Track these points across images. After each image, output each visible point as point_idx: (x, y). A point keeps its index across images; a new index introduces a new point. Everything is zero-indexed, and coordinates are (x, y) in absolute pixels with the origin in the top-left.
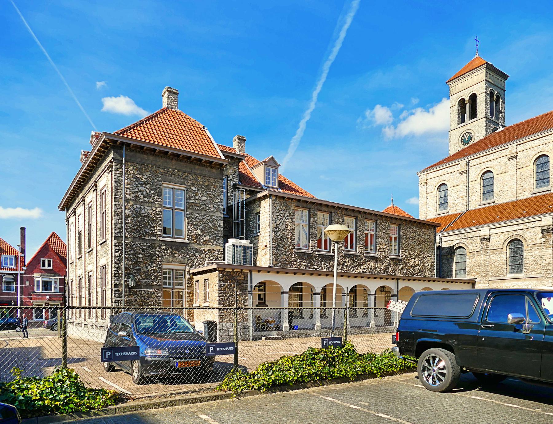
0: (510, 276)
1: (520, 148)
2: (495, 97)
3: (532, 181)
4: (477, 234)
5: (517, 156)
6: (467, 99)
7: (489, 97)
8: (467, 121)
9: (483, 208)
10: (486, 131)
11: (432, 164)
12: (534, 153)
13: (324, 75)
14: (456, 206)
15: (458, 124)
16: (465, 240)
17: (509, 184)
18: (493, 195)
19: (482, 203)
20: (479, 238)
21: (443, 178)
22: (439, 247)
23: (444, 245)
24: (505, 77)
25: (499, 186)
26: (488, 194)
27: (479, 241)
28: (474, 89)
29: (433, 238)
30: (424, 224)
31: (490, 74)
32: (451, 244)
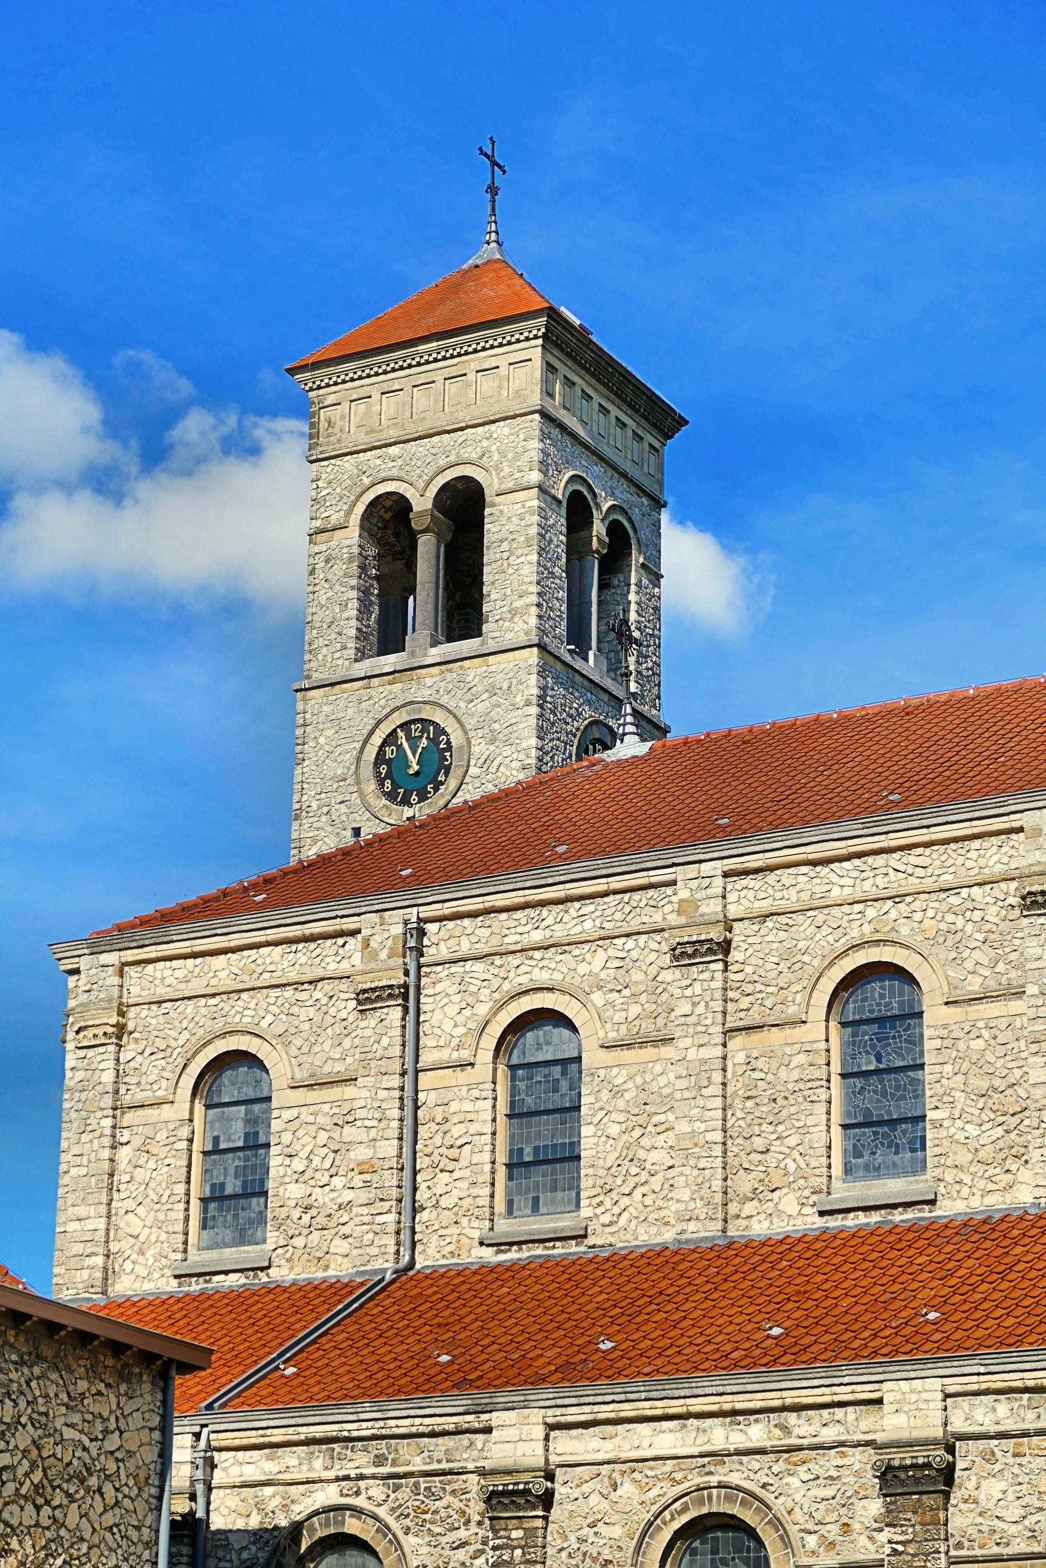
1: (745, 897)
2: (599, 528)
3: (817, 1127)
5: (726, 947)
6: (422, 502)
7: (562, 523)
8: (418, 636)
9: (512, 1269)
10: (541, 734)
11: (169, 904)
12: (827, 941)
14: (327, 1226)
15: (361, 655)
16: (377, 1491)
17: (683, 1127)
18: (574, 1185)
19: (505, 1226)
20: (474, 1478)
21: (244, 1011)
22: (189, 1530)
23: (226, 1514)
24: (661, 419)
25: (614, 1130)
26: (540, 1175)
27: (476, 1508)
28: (471, 453)
29: (151, 1454)
30: (84, 1338)
31: (569, 383)
32: (279, 1510)
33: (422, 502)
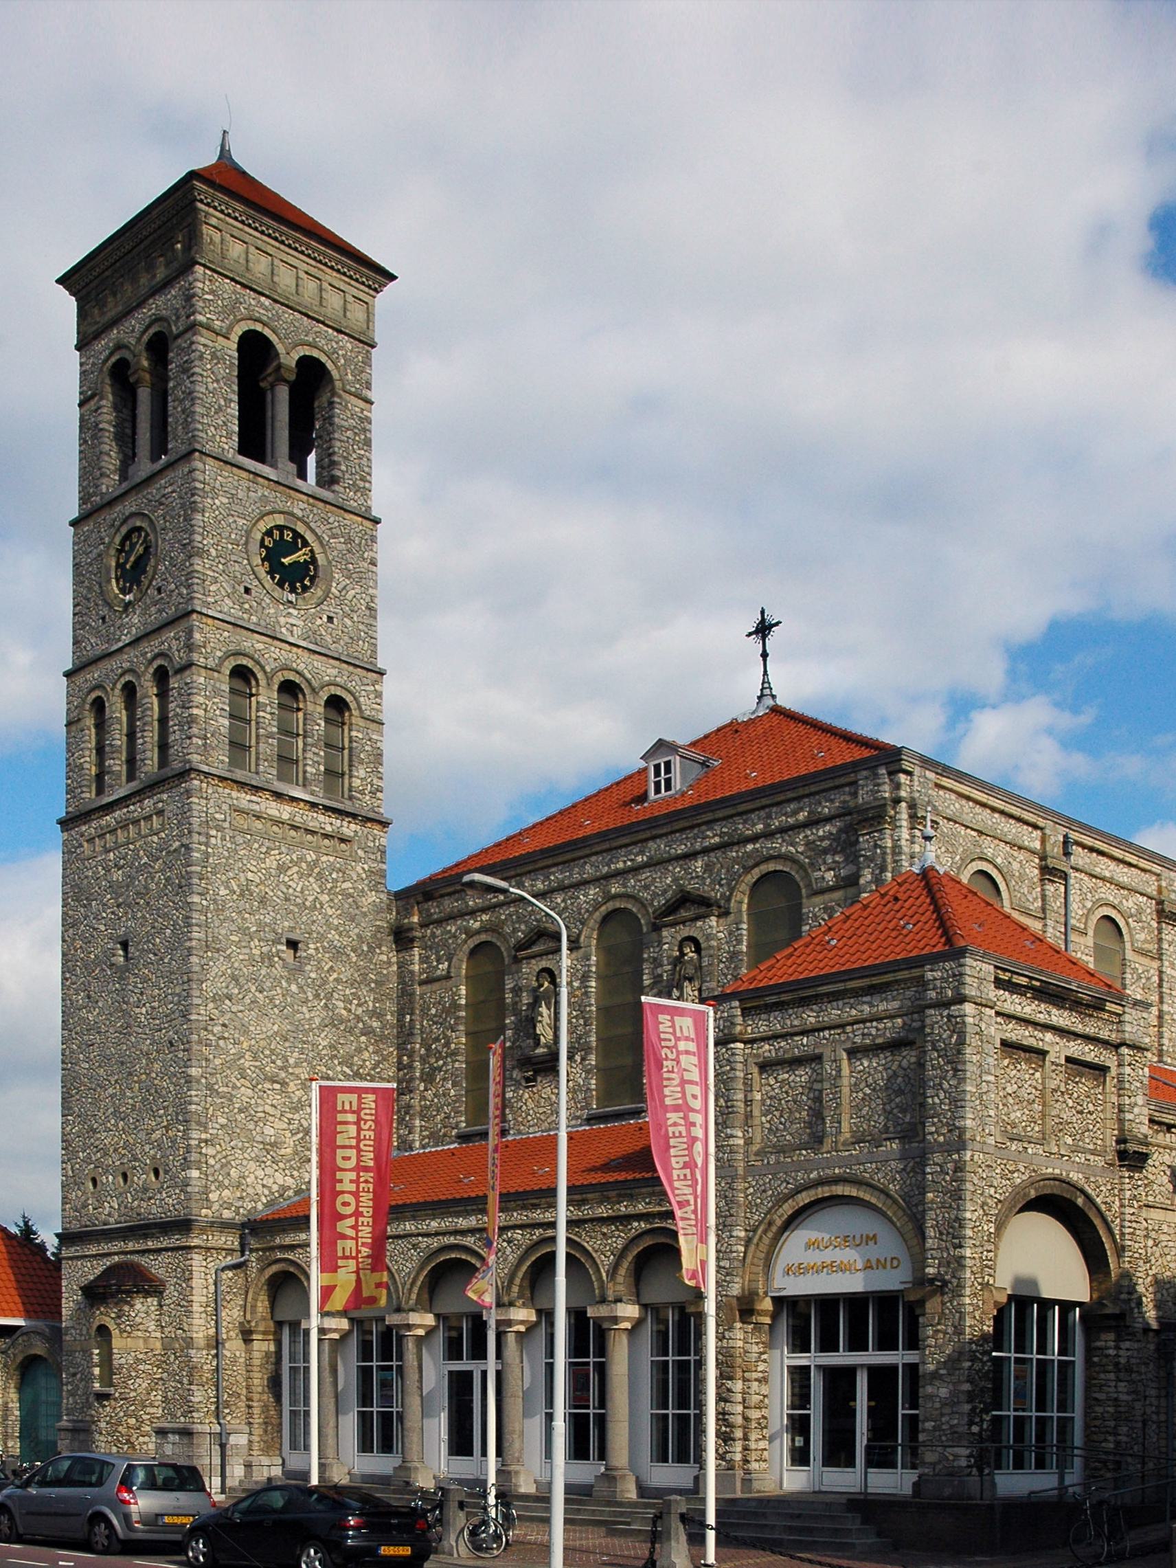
6: (289, 358)
33: (289, 358)
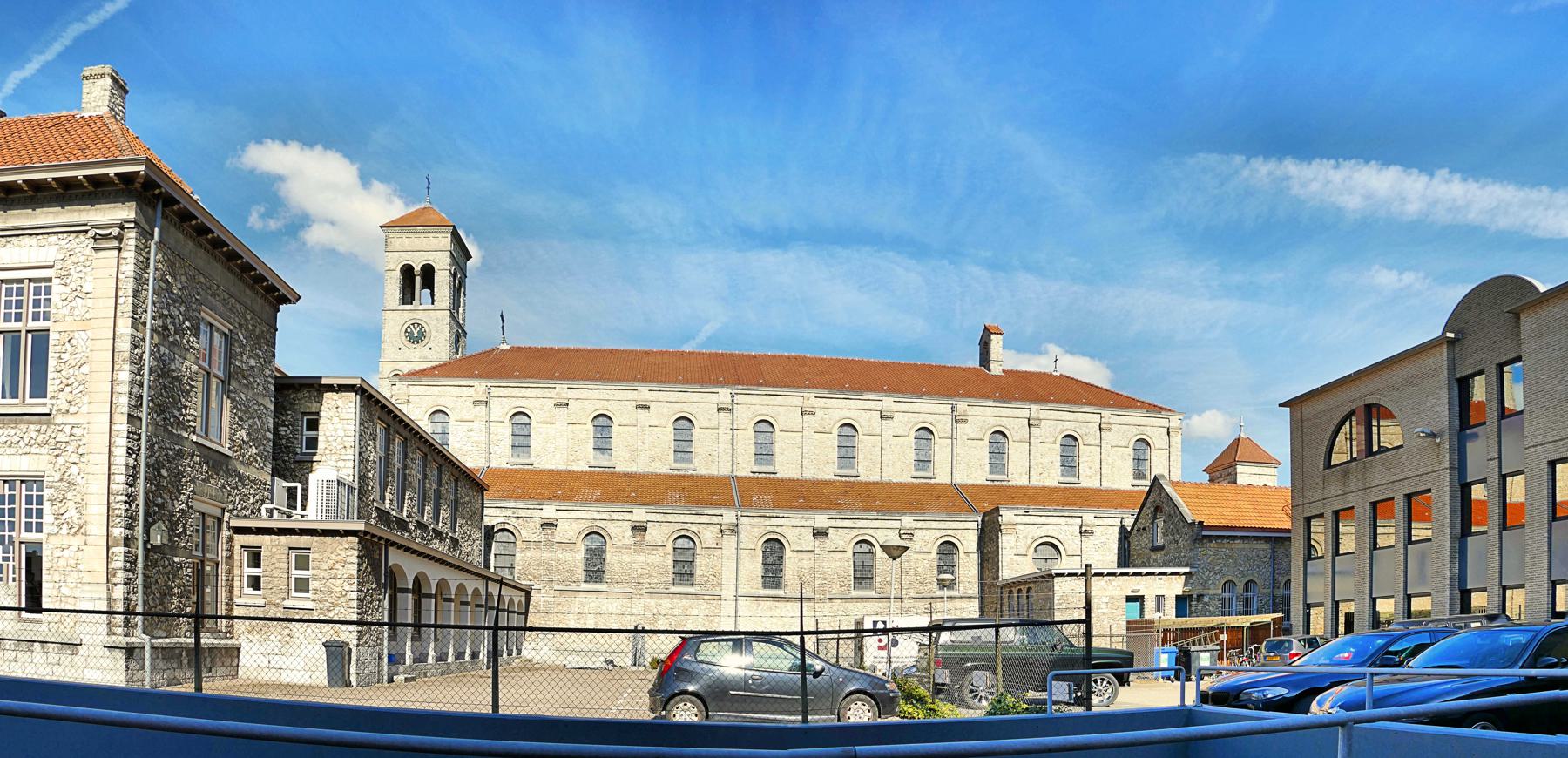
0: (855, 593)
1: (572, 394)
4: (537, 513)
6: (417, 269)
13: (57, 47)
33: (417, 269)
